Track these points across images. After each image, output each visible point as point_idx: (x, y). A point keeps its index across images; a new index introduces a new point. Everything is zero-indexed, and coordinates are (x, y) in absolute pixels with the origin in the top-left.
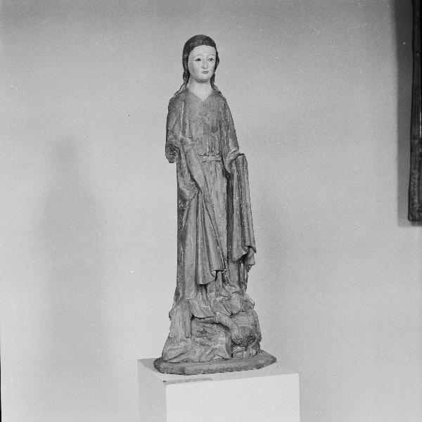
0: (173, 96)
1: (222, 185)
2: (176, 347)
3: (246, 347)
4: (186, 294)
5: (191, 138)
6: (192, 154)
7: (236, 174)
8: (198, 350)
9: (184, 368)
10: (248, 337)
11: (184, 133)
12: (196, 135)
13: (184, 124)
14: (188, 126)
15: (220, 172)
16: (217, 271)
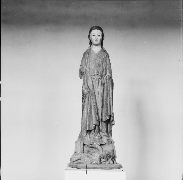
0: (85, 51)
1: (101, 89)
2: (77, 157)
3: (108, 160)
4: (82, 134)
5: (89, 68)
6: (89, 75)
7: (106, 83)
8: (87, 159)
9: (77, 165)
10: (107, 155)
11: (87, 67)
12: (92, 67)
13: (87, 62)
14: (88, 63)
15: (100, 84)
16: (95, 125)
